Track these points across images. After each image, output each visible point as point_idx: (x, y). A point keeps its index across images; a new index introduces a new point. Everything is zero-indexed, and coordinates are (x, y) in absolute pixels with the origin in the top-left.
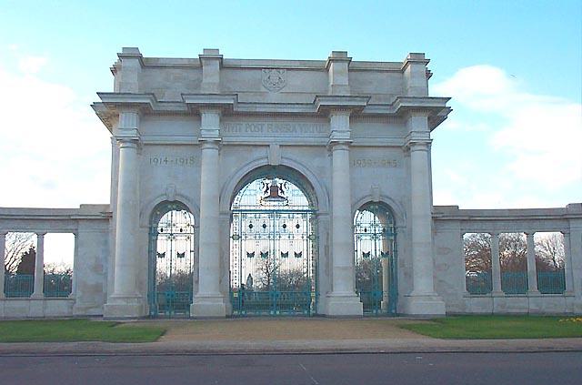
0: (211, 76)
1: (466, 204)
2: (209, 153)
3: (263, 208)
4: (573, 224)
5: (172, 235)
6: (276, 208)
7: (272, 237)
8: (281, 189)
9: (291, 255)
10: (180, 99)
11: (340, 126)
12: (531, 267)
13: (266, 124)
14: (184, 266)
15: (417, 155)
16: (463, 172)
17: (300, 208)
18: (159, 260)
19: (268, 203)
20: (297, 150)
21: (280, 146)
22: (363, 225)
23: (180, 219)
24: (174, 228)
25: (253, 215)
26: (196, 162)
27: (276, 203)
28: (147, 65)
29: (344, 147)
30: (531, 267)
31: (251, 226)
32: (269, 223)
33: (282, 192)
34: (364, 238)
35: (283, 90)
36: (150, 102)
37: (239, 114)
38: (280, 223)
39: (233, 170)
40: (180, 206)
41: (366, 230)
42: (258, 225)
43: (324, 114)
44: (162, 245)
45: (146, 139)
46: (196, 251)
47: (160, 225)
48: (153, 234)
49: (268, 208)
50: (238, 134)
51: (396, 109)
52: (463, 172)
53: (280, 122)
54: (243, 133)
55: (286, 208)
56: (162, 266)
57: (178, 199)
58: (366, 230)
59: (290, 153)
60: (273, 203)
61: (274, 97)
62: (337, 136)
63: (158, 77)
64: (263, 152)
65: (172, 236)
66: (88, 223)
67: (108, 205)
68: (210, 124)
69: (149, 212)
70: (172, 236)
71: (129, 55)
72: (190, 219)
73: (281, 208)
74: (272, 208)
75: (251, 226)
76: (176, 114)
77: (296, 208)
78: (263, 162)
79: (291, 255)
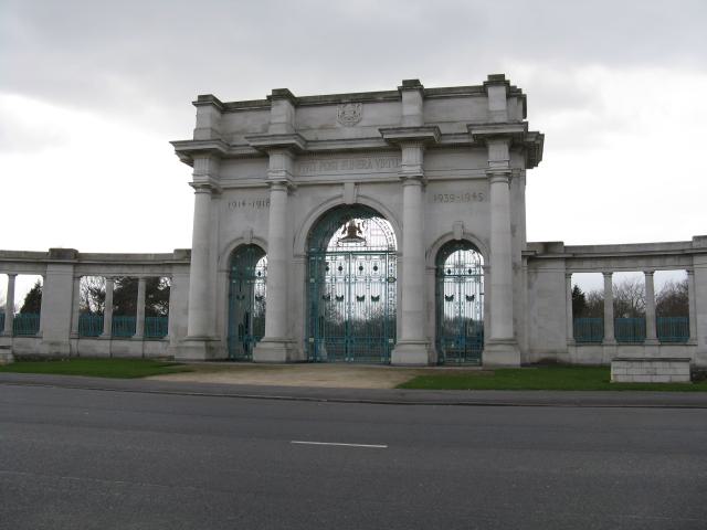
0: (411, 107)
1: (84, 248)
2: (277, 196)
3: (340, 249)
4: (697, 260)
5: (459, 276)
6: (354, 249)
7: (353, 280)
8: (359, 229)
9: (368, 299)
10: (380, 135)
11: (411, 159)
12: (609, 311)
13: (340, 161)
14: (472, 312)
15: (522, 182)
16: (561, 204)
17: (379, 249)
18: (446, 303)
19: (345, 244)
20: (373, 187)
21: (356, 184)
22: (468, 266)
23: (469, 258)
24: (462, 270)
25: (363, 257)
26: (482, 197)
27: (354, 244)
28: (225, 109)
29: (415, 182)
30: (609, 311)
31: (361, 268)
32: (345, 265)
33: (360, 232)
34: (468, 279)
35: (360, 124)
36: (223, 148)
37: (311, 153)
38: (355, 265)
39: (309, 209)
40: (466, 244)
41: (470, 271)
42: (368, 267)
43: (263, 154)
44: (449, 288)
45: (224, 183)
46: (487, 293)
47: (446, 266)
48: (440, 275)
49: (345, 249)
50: (313, 173)
51: (494, 137)
52: (561, 204)
53: (351, 160)
54: (318, 172)
55: (363, 249)
56: (450, 311)
57: (255, 242)
58: (470, 271)
59: (364, 191)
60: (350, 244)
61: (349, 133)
62: (406, 170)
63: (237, 121)
64: (335, 192)
65: (460, 279)
66: (180, 267)
67: (188, 251)
68: (278, 166)
69: (435, 251)
70: (460, 279)
71: (204, 101)
72: (479, 258)
73: (359, 249)
74: (349, 249)
75: (361, 268)
76: (250, 156)
77: (374, 249)
78: (338, 202)
79: (368, 299)
